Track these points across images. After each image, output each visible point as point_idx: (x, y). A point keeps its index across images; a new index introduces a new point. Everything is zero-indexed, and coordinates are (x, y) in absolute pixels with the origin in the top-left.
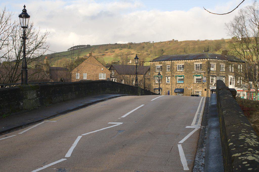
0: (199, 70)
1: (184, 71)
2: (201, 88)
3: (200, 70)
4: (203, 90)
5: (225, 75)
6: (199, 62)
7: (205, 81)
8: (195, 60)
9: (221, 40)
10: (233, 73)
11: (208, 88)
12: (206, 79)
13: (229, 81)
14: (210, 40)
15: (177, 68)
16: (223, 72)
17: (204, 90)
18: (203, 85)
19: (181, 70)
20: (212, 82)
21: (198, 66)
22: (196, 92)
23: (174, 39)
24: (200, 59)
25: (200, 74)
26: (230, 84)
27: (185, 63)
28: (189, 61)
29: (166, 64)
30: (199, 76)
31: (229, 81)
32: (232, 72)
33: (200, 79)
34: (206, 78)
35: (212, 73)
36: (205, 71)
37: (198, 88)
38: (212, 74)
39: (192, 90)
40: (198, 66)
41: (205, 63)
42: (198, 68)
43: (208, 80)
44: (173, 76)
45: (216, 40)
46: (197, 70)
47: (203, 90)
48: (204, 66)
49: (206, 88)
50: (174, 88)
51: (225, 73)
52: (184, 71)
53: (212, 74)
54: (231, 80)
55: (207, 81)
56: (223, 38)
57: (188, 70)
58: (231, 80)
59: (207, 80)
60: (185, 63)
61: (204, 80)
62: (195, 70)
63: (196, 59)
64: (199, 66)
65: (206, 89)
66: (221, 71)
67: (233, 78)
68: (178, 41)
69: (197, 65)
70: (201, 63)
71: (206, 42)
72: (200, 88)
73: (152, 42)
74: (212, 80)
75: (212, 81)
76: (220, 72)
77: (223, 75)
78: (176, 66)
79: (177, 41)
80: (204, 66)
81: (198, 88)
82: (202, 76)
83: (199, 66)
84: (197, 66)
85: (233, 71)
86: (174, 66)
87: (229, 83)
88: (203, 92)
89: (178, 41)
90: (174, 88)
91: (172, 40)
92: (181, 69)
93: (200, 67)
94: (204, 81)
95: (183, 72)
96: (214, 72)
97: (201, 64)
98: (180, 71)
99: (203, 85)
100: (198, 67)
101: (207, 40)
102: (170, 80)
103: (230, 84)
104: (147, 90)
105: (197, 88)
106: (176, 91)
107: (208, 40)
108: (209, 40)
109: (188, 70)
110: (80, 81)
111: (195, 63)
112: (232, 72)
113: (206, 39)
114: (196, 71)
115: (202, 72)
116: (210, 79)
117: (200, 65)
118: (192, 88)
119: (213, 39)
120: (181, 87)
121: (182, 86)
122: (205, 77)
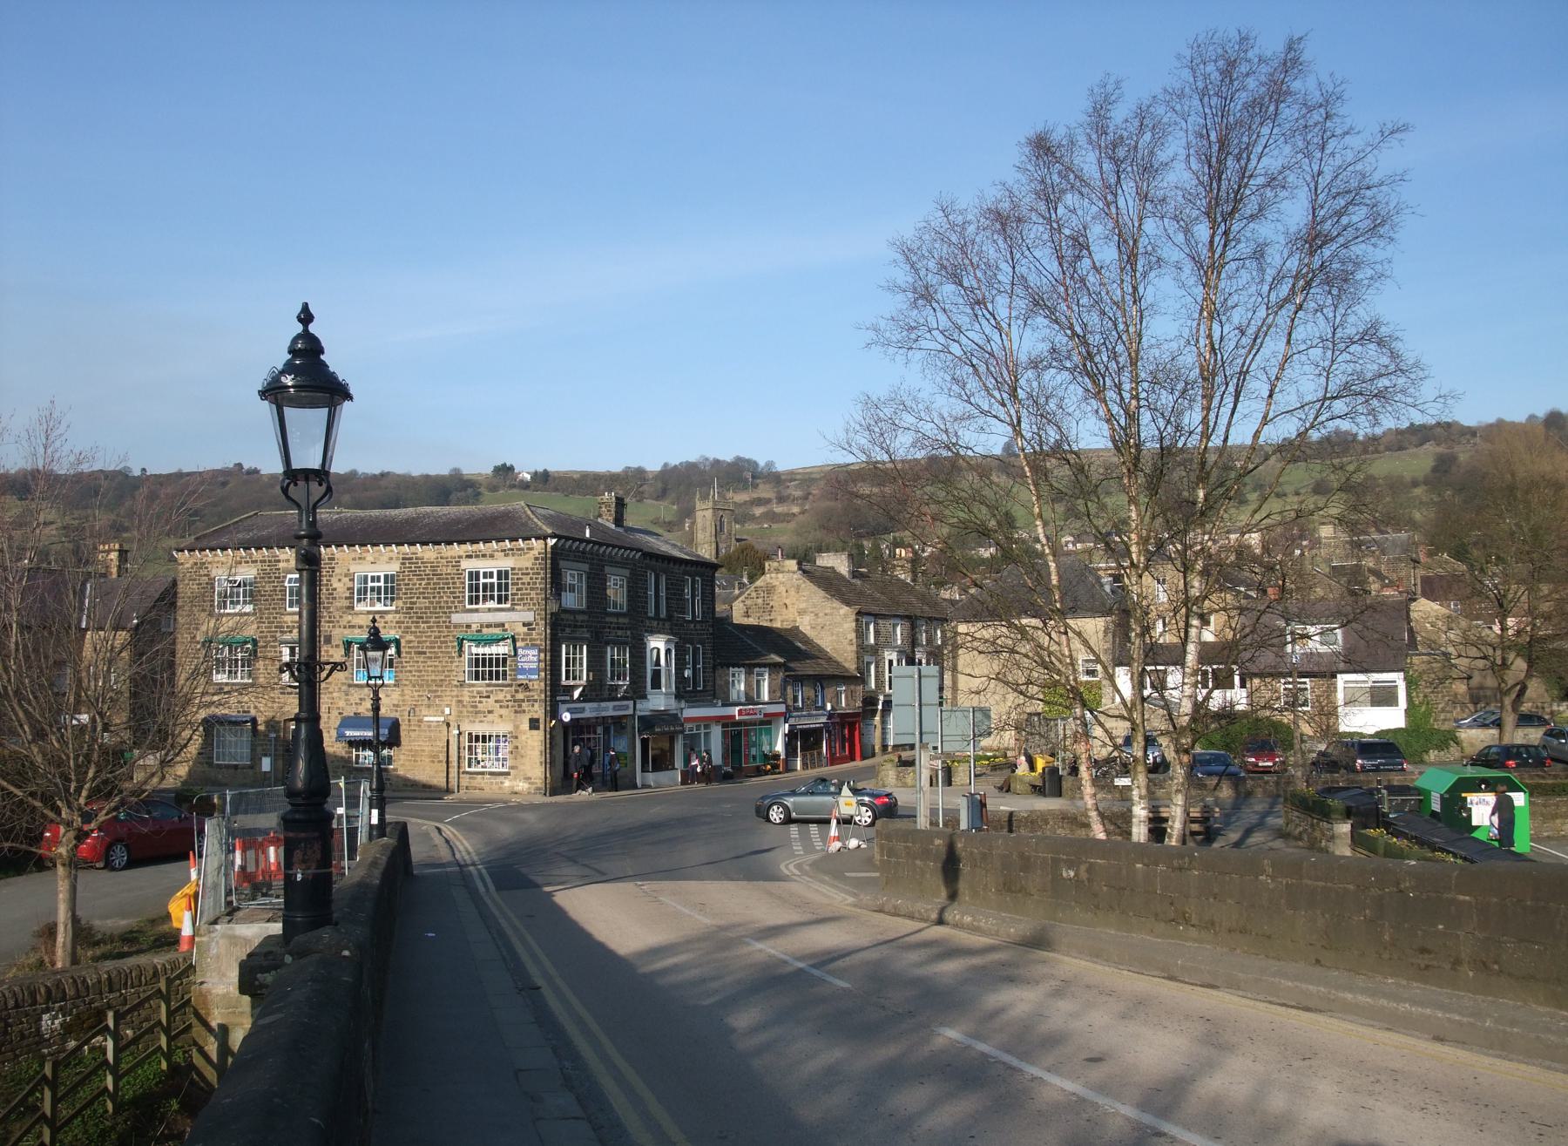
1: (397, 612)
2: (504, 711)
4: (517, 727)
6: (492, 556)
7: (531, 671)
8: (468, 547)
9: (451, 475)
16: (621, 620)
17: (526, 726)
18: (520, 696)
21: (376, 584)
23: (240, 465)
24: (499, 540)
25: (497, 631)
27: (405, 559)
28: (428, 553)
29: (281, 565)
30: (497, 641)
32: (657, 617)
33: (497, 659)
34: (540, 651)
35: (570, 626)
37: (490, 712)
38: (568, 630)
39: (448, 725)
40: (376, 584)
41: (526, 562)
42: (484, 591)
45: (427, 476)
47: (517, 727)
48: (526, 579)
50: (335, 713)
51: (626, 621)
52: (397, 612)
53: (568, 630)
56: (455, 469)
57: (422, 603)
60: (405, 559)
61: (526, 666)
62: (468, 607)
63: (412, 544)
64: (495, 580)
65: (537, 720)
68: (262, 473)
69: (366, 577)
70: (506, 563)
71: (383, 483)
73: (137, 473)
76: (608, 619)
77: (620, 633)
79: (256, 471)
80: (526, 579)
81: (490, 712)
82: (514, 640)
83: (492, 584)
84: (366, 582)
85: (663, 614)
86: (334, 580)
88: (523, 738)
89: (262, 473)
90: (335, 713)
91: (231, 466)
92: (492, 598)
94: (523, 671)
95: (389, 617)
96: (580, 618)
99: (520, 696)
100: (485, 585)
101: (388, 473)
104: (593, 791)
105: (479, 712)
106: (348, 733)
107: (394, 474)
108: (398, 476)
109: (422, 603)
113: (386, 471)
117: (386, 582)
118: (447, 711)
119: (416, 472)
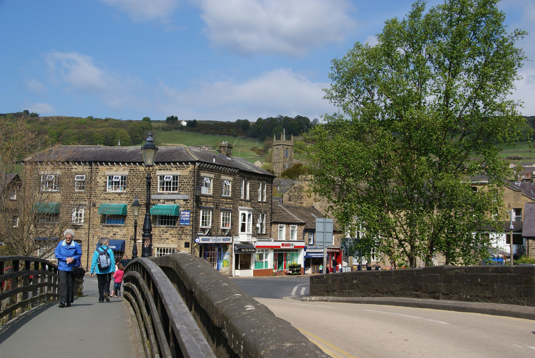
0: (170, 190)
1: (126, 193)
2: (173, 239)
3: (172, 192)
5: (231, 206)
7: (187, 221)
10: (248, 201)
11: (193, 241)
12: (190, 217)
13: (240, 221)
14: (118, 120)
15: (105, 182)
17: (183, 246)
19: (119, 191)
20: (203, 225)
21: (116, 180)
22: (161, 252)
26: (242, 231)
31: (240, 221)
34: (191, 213)
35: (204, 202)
36: (187, 197)
37: (167, 239)
43: (195, 220)
44: (94, 205)
46: (165, 192)
47: (179, 246)
48: (186, 180)
49: (189, 239)
54: (244, 220)
55: (193, 221)
58: (244, 220)
59: (191, 219)
61: (184, 219)
62: (159, 192)
65: (188, 243)
66: (223, 195)
67: (249, 215)
72: (171, 239)
74: (203, 219)
75: (203, 222)
77: (227, 206)
78: (103, 178)
79: (36, 115)
80: (186, 180)
81: (167, 239)
87: (238, 228)
89: (40, 116)
93: (174, 185)
95: (123, 196)
97: (125, 177)
98: (114, 193)
102: (83, 216)
103: (242, 231)
105: (162, 239)
110: (169, 315)
111: (159, 173)
112: (245, 200)
114: (163, 194)
115: (179, 197)
116: (199, 215)
120: (118, 237)
121: (120, 233)
122: (188, 211)
